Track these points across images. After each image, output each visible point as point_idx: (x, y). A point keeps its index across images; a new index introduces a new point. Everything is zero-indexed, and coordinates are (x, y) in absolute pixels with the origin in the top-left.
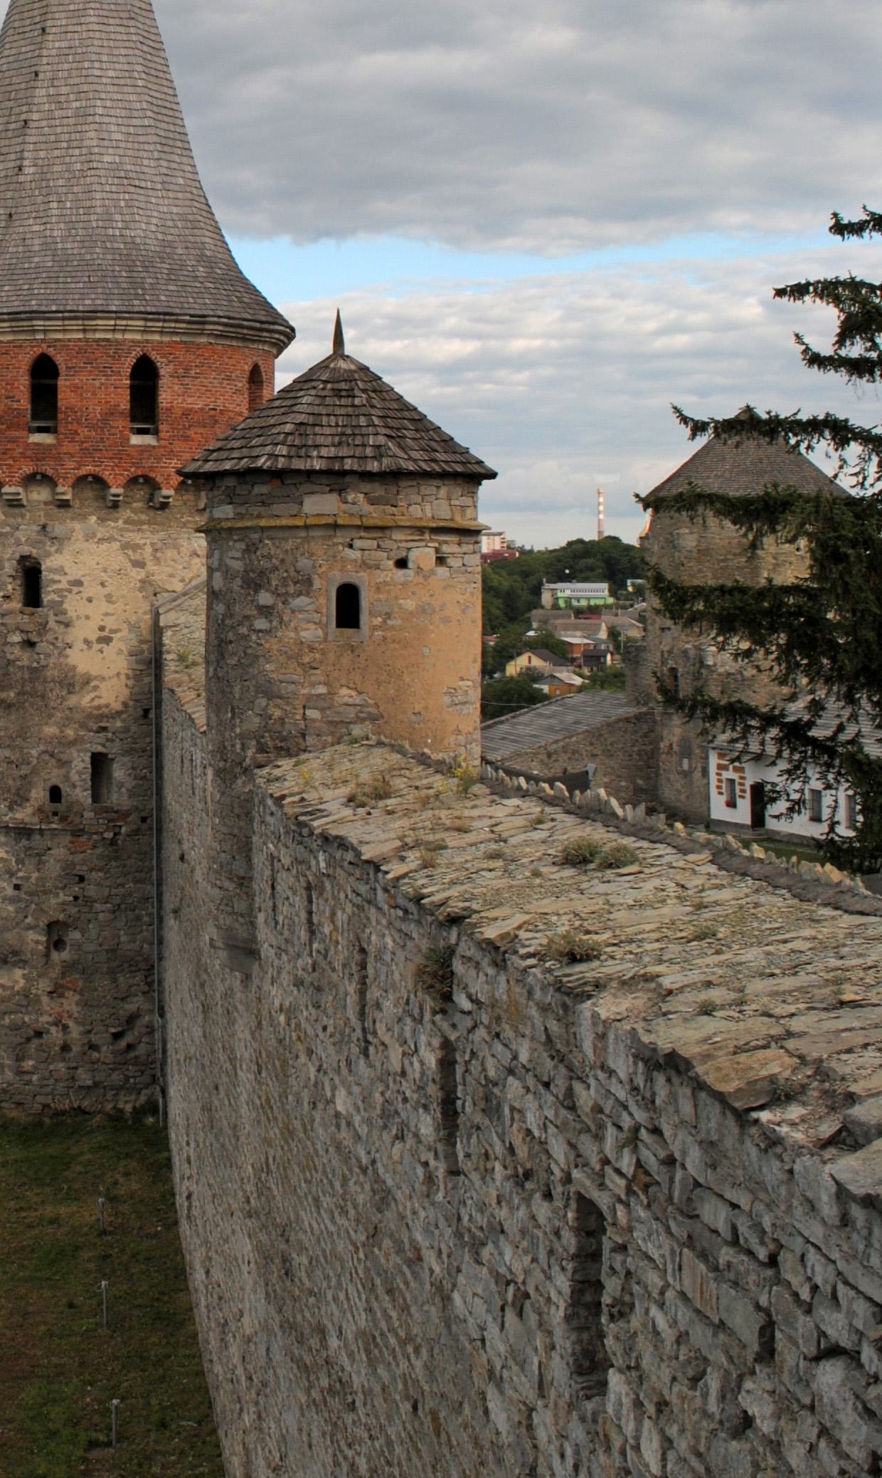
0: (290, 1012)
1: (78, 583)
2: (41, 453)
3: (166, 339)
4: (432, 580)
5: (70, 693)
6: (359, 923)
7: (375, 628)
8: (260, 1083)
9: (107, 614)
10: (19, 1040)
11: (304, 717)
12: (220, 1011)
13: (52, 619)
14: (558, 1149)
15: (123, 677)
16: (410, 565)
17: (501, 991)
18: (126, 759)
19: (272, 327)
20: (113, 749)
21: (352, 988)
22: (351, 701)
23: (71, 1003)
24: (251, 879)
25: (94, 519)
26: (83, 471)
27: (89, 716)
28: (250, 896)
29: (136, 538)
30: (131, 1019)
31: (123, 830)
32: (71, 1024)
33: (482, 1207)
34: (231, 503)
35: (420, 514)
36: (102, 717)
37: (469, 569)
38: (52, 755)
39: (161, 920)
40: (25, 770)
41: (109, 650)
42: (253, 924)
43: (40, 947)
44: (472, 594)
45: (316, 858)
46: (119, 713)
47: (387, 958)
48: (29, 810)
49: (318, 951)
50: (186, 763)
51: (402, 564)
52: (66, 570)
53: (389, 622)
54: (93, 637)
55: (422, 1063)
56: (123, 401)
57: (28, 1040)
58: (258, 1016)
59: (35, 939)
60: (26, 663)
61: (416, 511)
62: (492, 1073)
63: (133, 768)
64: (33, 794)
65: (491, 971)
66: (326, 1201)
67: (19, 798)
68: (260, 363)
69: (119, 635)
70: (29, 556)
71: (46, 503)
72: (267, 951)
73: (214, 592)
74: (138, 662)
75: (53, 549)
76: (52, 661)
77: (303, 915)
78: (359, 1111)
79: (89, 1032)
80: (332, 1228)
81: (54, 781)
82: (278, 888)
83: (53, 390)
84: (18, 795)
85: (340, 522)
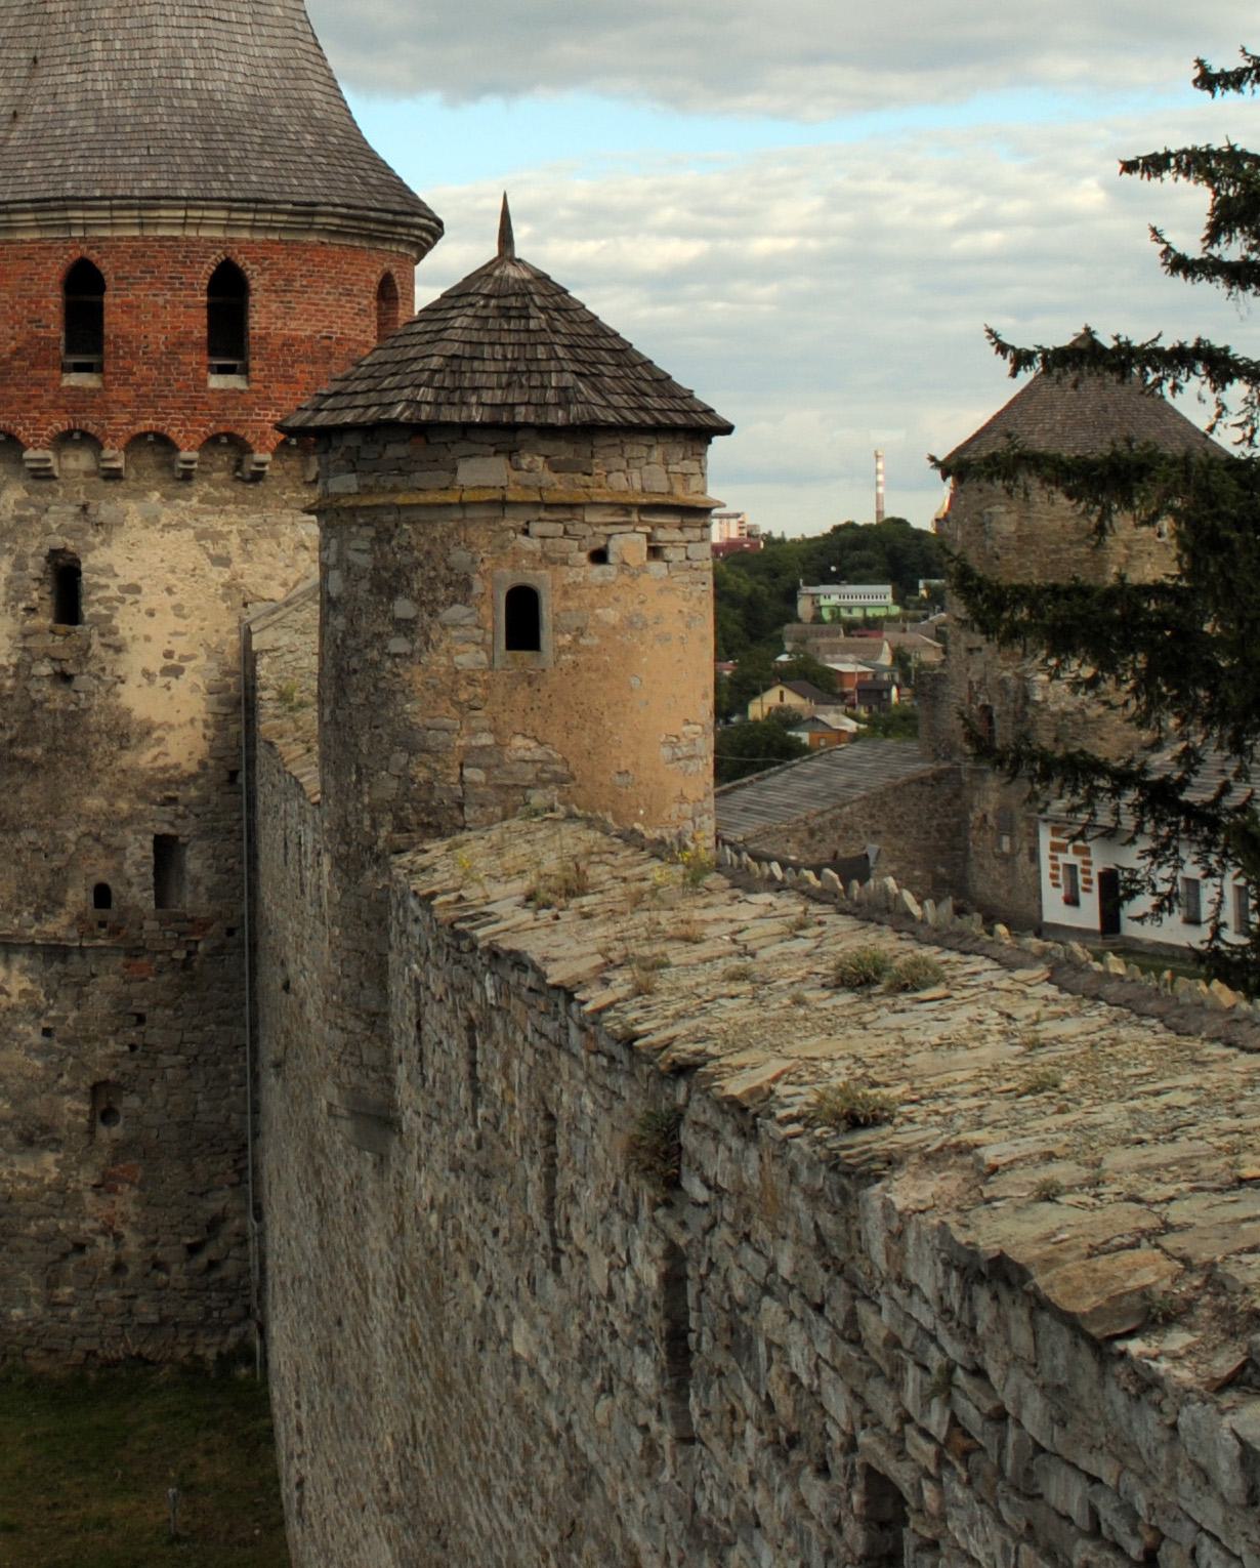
0: (446, 1209)
1: (135, 589)
2: (79, 401)
3: (259, 237)
4: (643, 580)
5: (122, 748)
7: (562, 650)
8: (402, 1315)
9: (176, 634)
10: (50, 1257)
11: (462, 780)
12: (343, 1209)
13: (96, 641)
14: (837, 1402)
15: (199, 725)
16: (611, 558)
18: (204, 844)
19: (409, 219)
20: (186, 830)
22: (528, 756)
23: (126, 1201)
24: (386, 1015)
27: (151, 782)
28: (386, 1040)
29: (218, 523)
30: (214, 1225)
31: (201, 947)
32: (126, 1232)
33: (728, 1490)
35: (624, 485)
37: (696, 564)
38: (97, 839)
39: (256, 1077)
40: (58, 861)
41: (180, 686)
44: (700, 600)
45: (481, 983)
46: (193, 777)
47: (586, 1126)
48: (64, 920)
50: (292, 848)
51: (599, 557)
53: (582, 641)
54: (156, 666)
55: (638, 1280)
56: (198, 327)
57: (65, 1256)
59: (73, 1108)
60: (59, 704)
61: (618, 481)
64: (71, 896)
65: (736, 1143)
66: (501, 1487)
67: (51, 902)
70: (64, 551)
71: (87, 474)
72: (410, 1120)
73: (330, 600)
74: (220, 703)
75: (98, 540)
76: (96, 701)
77: (463, 1067)
78: (546, 1353)
79: (154, 1243)
80: (509, 1526)
81: (101, 877)
82: (427, 1028)
83: (98, 309)
84: (48, 897)
85: (510, 497)
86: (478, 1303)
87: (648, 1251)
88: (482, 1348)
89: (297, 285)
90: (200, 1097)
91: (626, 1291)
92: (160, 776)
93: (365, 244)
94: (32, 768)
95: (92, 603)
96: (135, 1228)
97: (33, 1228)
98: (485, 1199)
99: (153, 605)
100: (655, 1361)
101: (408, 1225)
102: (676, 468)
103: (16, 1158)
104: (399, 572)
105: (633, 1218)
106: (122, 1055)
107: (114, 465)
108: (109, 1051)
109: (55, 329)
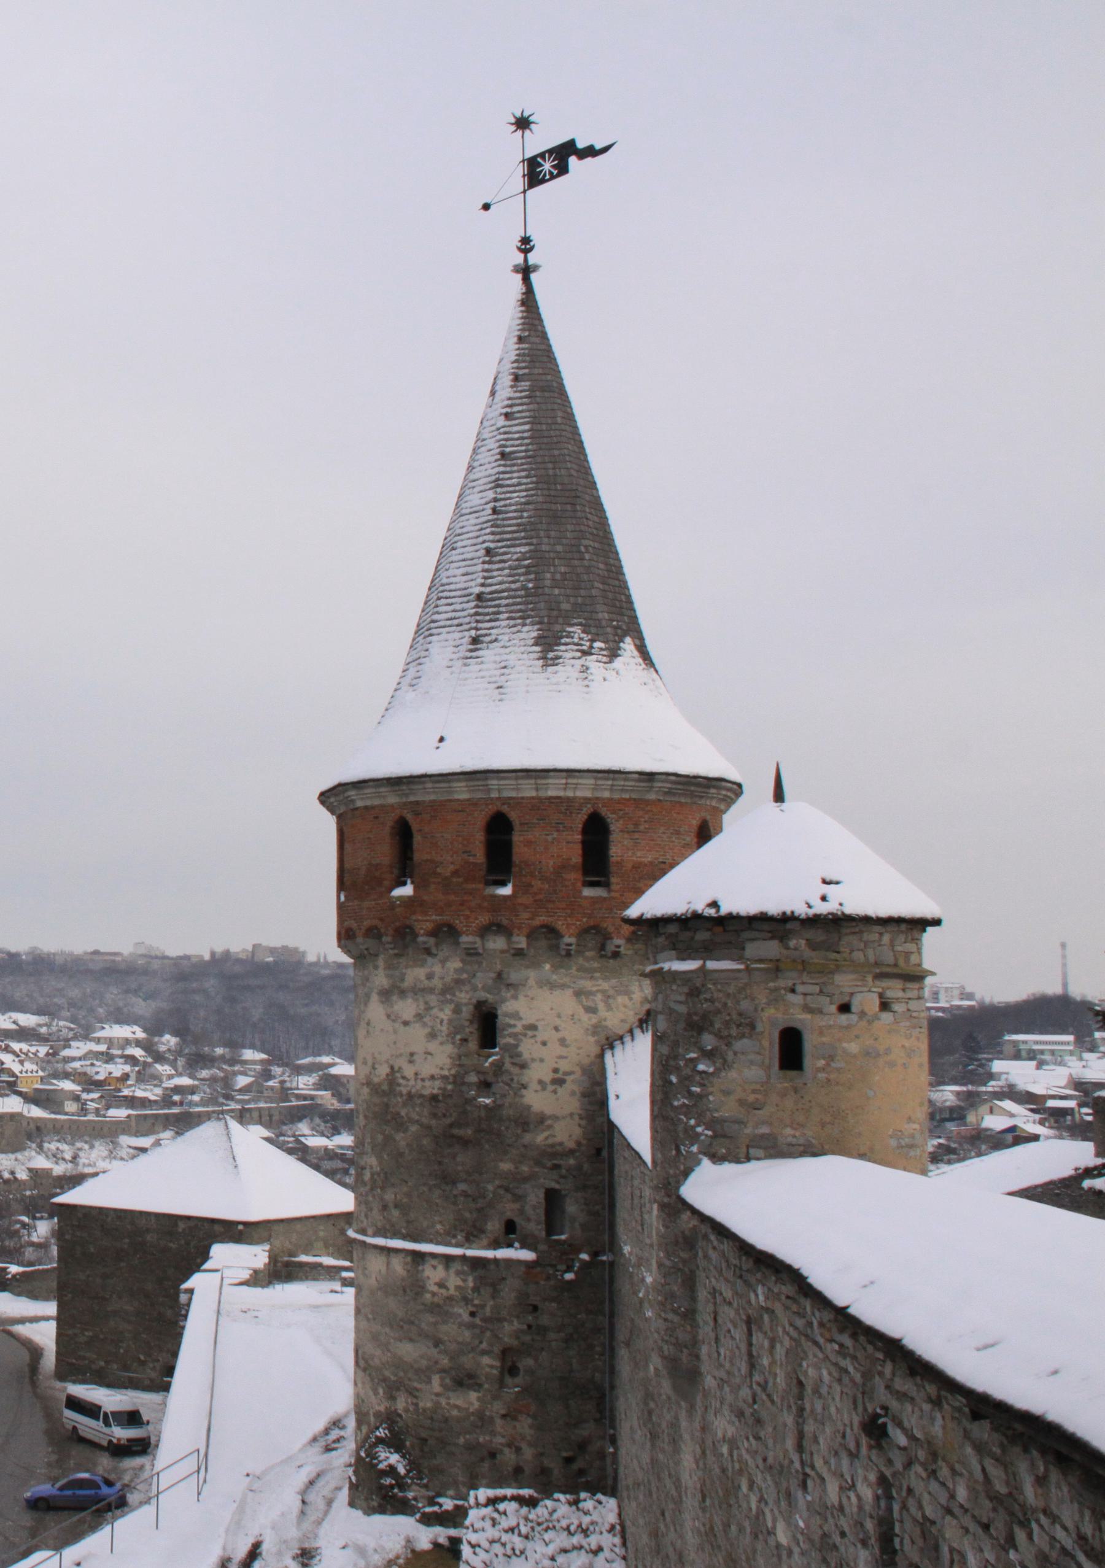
0: (733, 1444)
1: (533, 1027)
4: (876, 1024)
5: (524, 1131)
6: (795, 1355)
7: (819, 1070)
9: (561, 1057)
12: (666, 1440)
15: (576, 1117)
16: (854, 1009)
17: (937, 1429)
18: (579, 1194)
21: (789, 1419)
23: (525, 1426)
25: (547, 967)
26: (537, 922)
28: (695, 1326)
29: (587, 984)
30: (582, 1446)
32: (524, 1446)
34: (674, 949)
36: (554, 1155)
37: (914, 1014)
38: (507, 1190)
39: (612, 1349)
40: (481, 1203)
42: (697, 1357)
43: (495, 1372)
45: (755, 1292)
46: (572, 1152)
47: (824, 1390)
49: (759, 1384)
50: (636, 1201)
51: (845, 1008)
52: (521, 1014)
53: (833, 1065)
54: (548, 1077)
56: (575, 855)
58: (703, 1443)
59: (488, 1363)
62: (929, 1512)
63: (586, 1204)
64: (489, 1226)
65: (927, 1407)
68: (708, 817)
69: (572, 1077)
70: (486, 1001)
71: (503, 952)
75: (509, 995)
76: (508, 1100)
77: (744, 1347)
78: (798, 1544)
81: (509, 1215)
82: (720, 1321)
86: (754, 1506)
87: (866, 1478)
88: (756, 1537)
89: (642, 828)
90: (574, 1361)
91: (851, 1504)
92: (549, 1150)
93: (689, 801)
94: (465, 1143)
95: (504, 1037)
96: (530, 1445)
97: (461, 1441)
98: (757, 1438)
99: (545, 1038)
100: (871, 1554)
101: (708, 1452)
102: (899, 948)
103: (451, 1394)
104: (705, 1016)
105: (853, 1455)
106: (522, 1331)
107: (520, 946)
108: (514, 1328)
109: (479, 856)
